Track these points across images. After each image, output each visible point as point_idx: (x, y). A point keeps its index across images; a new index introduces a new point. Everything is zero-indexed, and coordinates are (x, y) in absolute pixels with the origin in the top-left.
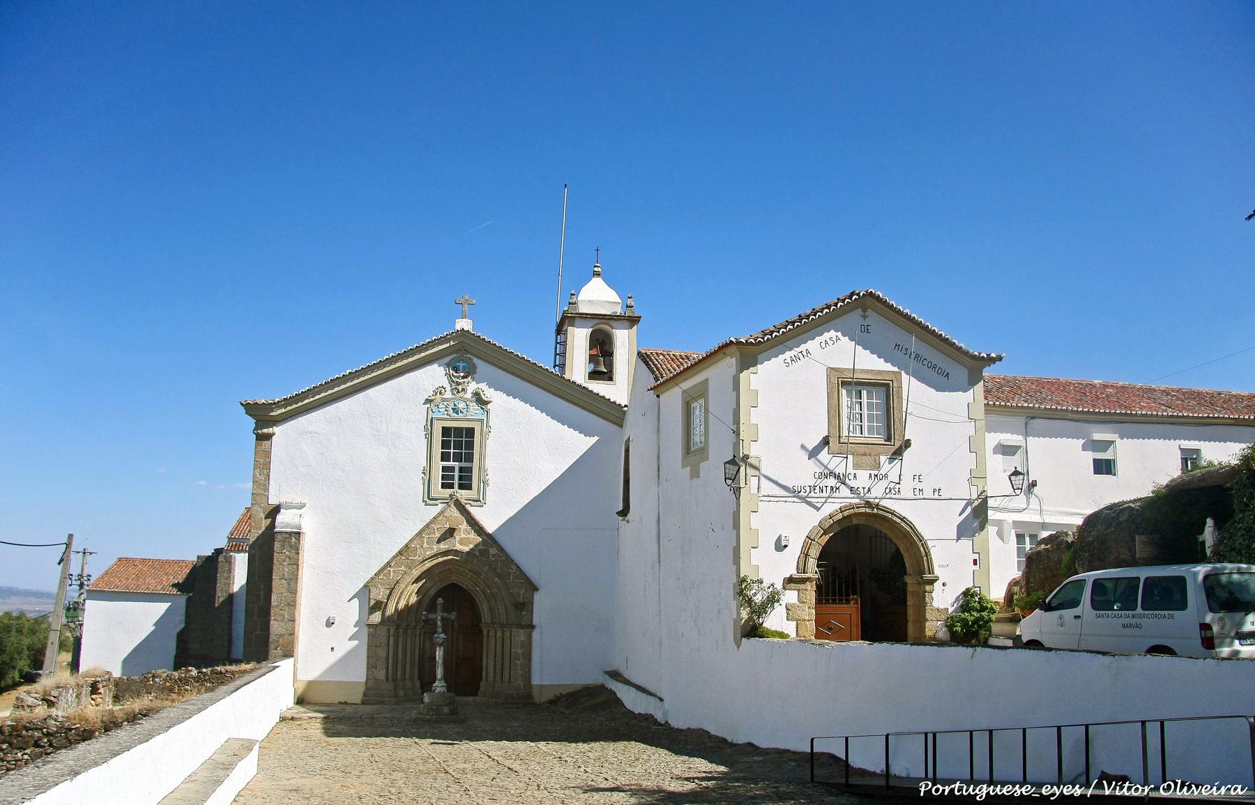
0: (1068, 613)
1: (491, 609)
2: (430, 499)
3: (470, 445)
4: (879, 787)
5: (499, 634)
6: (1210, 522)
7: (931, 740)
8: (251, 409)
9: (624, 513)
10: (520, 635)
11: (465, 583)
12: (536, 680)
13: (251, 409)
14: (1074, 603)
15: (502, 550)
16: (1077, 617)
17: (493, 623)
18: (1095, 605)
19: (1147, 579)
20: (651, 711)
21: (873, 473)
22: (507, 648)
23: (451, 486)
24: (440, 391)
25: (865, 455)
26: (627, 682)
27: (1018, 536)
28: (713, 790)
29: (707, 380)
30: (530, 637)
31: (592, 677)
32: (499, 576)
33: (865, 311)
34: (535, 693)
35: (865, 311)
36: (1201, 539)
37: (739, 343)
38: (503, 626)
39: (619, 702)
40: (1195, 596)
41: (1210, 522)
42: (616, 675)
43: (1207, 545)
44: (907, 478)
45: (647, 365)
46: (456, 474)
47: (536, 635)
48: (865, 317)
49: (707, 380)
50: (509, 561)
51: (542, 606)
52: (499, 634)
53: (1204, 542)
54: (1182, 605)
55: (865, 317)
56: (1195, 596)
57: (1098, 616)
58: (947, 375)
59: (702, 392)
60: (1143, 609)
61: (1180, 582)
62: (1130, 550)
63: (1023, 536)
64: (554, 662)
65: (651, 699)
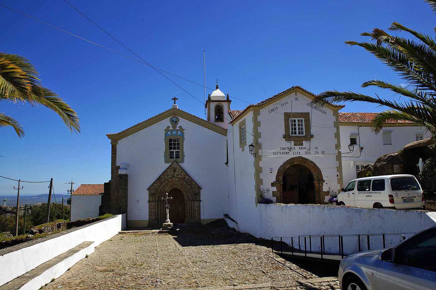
0: (351, 192)
1: (187, 196)
2: (166, 162)
3: (170, 144)
4: (291, 255)
5: (190, 203)
6: (421, 159)
7: (322, 239)
8: (109, 136)
9: (227, 163)
10: (197, 203)
11: (179, 187)
12: (202, 218)
13: (109, 136)
14: (353, 189)
15: (190, 177)
16: (353, 193)
17: (188, 200)
18: (359, 190)
19: (374, 180)
20: (235, 227)
21: (301, 147)
22: (193, 208)
23: (173, 157)
24: (168, 127)
25: (298, 142)
26: (230, 218)
27: (179, 157)
28: (371, 259)
29: (245, 119)
30: (199, 204)
31: (221, 217)
32: (189, 185)
33: (296, 93)
34: (202, 221)
35: (296, 93)
36: (418, 165)
37: (253, 106)
38: (191, 201)
39: (227, 224)
40: (388, 185)
41: (421, 159)
42: (227, 216)
43: (420, 167)
44: (312, 147)
45: (230, 116)
46: (175, 154)
47: (201, 203)
48: (296, 95)
49: (245, 119)
50: (192, 180)
51: (203, 195)
52: (190, 203)
53: (419, 167)
54: (383, 189)
55: (296, 95)
56: (388, 185)
57: (359, 193)
58: (326, 113)
59: (244, 123)
60: (372, 190)
61: (383, 181)
62: (392, 170)
63: (176, 157)
64: (208, 211)
65: (234, 223)
